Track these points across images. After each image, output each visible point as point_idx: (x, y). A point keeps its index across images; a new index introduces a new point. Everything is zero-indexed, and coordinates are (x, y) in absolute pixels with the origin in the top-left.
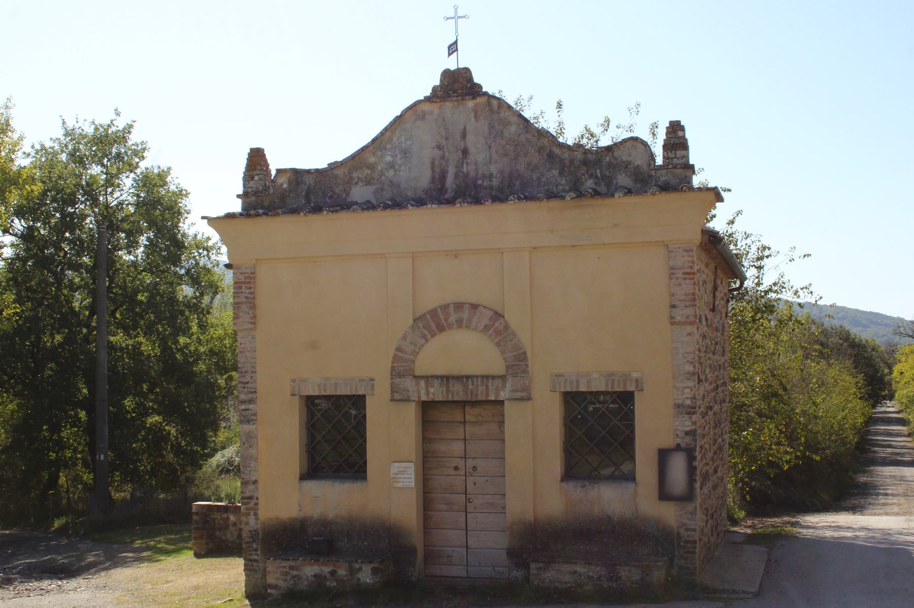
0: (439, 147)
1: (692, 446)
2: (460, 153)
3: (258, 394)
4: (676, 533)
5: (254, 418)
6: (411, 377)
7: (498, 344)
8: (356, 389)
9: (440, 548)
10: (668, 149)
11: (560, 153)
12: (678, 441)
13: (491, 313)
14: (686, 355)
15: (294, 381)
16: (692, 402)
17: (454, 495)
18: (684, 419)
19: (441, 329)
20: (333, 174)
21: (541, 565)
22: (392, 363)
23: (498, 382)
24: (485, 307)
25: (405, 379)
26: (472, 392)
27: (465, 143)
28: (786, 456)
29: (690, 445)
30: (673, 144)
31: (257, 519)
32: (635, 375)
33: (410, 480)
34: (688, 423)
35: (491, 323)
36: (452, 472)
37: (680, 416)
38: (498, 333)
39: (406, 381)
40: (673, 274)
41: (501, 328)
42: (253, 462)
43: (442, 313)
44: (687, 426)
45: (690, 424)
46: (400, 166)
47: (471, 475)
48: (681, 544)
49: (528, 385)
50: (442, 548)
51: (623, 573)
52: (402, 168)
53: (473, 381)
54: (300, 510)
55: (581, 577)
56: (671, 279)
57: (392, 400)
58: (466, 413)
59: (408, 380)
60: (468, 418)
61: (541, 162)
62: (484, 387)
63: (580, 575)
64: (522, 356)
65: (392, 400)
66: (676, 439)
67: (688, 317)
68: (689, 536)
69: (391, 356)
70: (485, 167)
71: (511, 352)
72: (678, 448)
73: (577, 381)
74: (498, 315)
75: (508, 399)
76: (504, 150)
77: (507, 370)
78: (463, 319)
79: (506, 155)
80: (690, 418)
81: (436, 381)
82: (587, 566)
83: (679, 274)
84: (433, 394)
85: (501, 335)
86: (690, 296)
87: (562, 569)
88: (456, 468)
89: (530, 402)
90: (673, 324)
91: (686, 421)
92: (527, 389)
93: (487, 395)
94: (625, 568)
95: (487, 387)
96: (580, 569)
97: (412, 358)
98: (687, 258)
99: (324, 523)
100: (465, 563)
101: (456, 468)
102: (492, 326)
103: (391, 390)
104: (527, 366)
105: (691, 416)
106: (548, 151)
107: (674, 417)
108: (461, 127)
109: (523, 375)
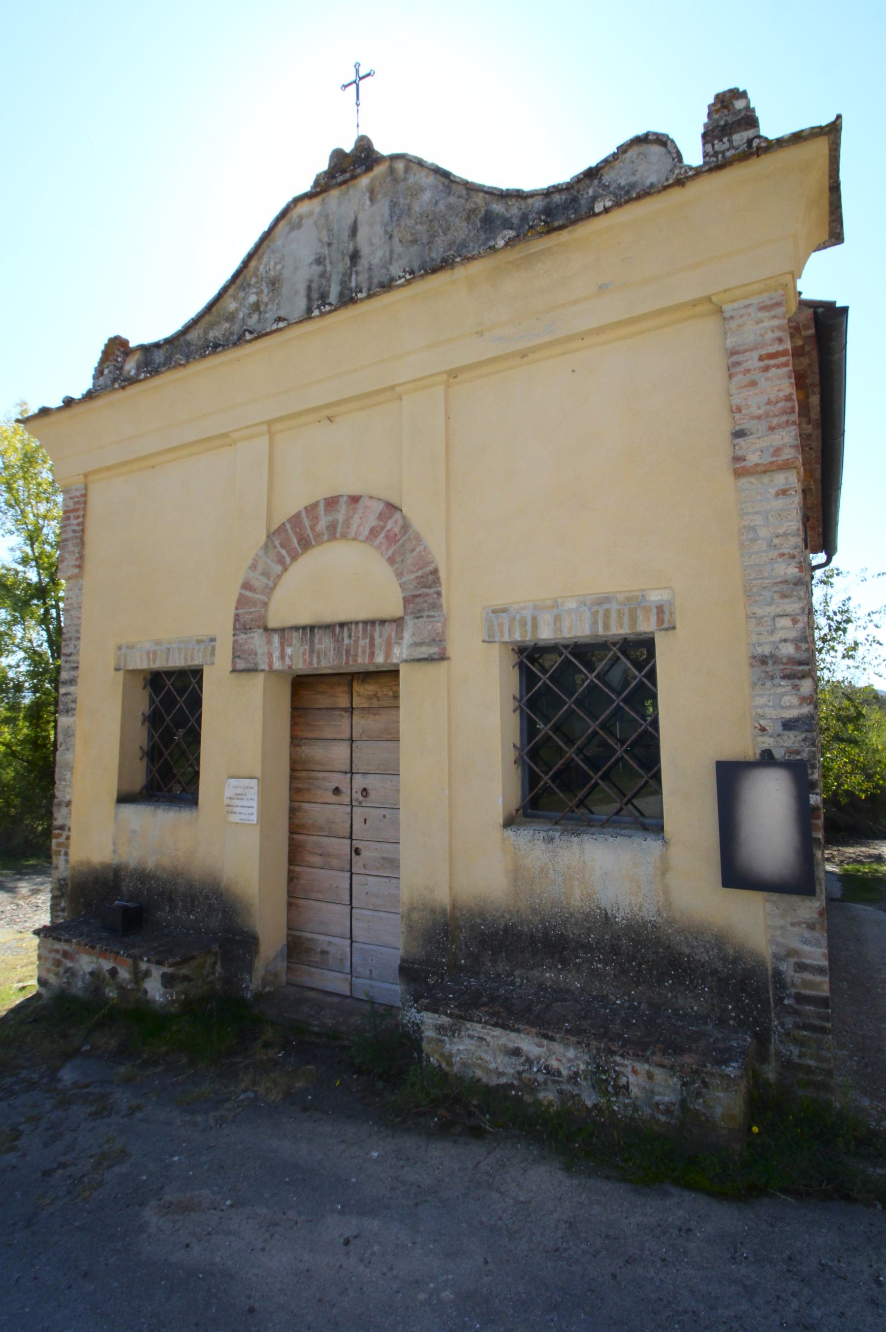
0: (319, 261)
1: (805, 755)
2: (348, 260)
3: (80, 671)
4: (770, 972)
5: (73, 705)
6: (261, 631)
7: (391, 561)
8: (192, 657)
9: (309, 935)
10: (714, 138)
11: (503, 210)
12: (767, 742)
13: (381, 506)
14: (776, 541)
15: (120, 648)
16: (798, 648)
17: (333, 840)
18: (780, 690)
19: (306, 544)
20: (185, 340)
21: (445, 1020)
22: (237, 609)
23: (390, 629)
24: (371, 498)
25: (252, 635)
26: (348, 652)
27: (355, 243)
28: (854, 782)
29: (798, 752)
30: (724, 128)
31: (67, 861)
32: (655, 597)
33: (250, 811)
34: (791, 699)
35: (381, 523)
36: (330, 797)
37: (769, 684)
38: (391, 539)
39: (252, 638)
40: (738, 364)
41: (397, 530)
42: (69, 773)
43: (308, 517)
44: (790, 707)
45: (795, 701)
46: (266, 305)
47: (360, 805)
48: (786, 1002)
49: (440, 631)
50: (315, 936)
51: (632, 1079)
52: (269, 307)
53: (349, 630)
54: (114, 852)
55: (531, 1067)
56: (731, 376)
57: (234, 671)
58: (355, 694)
59: (256, 635)
60: (357, 702)
61: (471, 235)
62: (367, 641)
63: (529, 1061)
64: (431, 577)
65: (234, 671)
66: (760, 739)
67: (777, 451)
68: (806, 984)
69: (235, 597)
70: (383, 271)
71: (413, 572)
72: (767, 759)
73: (534, 619)
74: (392, 508)
75: (406, 661)
76: (412, 234)
77: (405, 607)
78: (337, 521)
79: (415, 241)
80: (796, 687)
81: (295, 634)
82: (545, 1042)
83: (752, 361)
84: (291, 658)
85: (396, 542)
86: (782, 404)
87: (488, 1039)
88: (337, 791)
89: (444, 664)
90: (739, 473)
91: (785, 694)
92: (439, 640)
93: (372, 654)
94: (638, 1066)
95: (372, 639)
96: (529, 1044)
97: (264, 598)
98: (767, 324)
99: (142, 876)
100: (348, 970)
101: (337, 791)
102: (383, 528)
103: (233, 654)
104: (439, 594)
105: (797, 682)
106: (483, 211)
107: (754, 685)
108: (350, 221)
109: (433, 613)
